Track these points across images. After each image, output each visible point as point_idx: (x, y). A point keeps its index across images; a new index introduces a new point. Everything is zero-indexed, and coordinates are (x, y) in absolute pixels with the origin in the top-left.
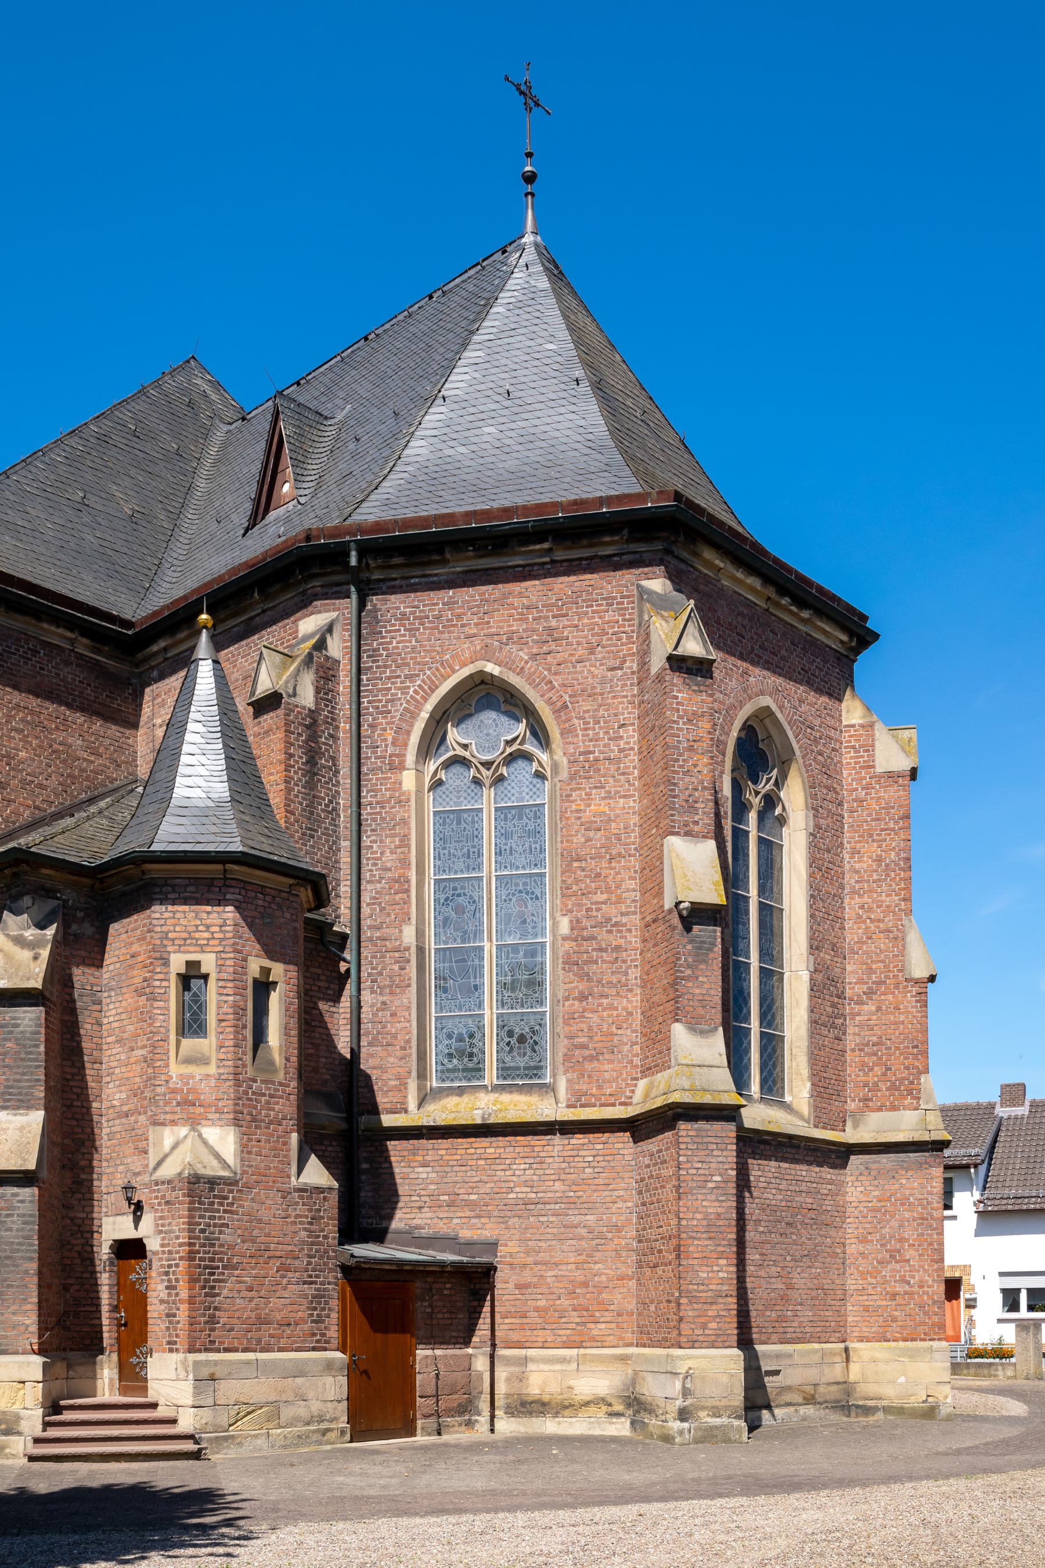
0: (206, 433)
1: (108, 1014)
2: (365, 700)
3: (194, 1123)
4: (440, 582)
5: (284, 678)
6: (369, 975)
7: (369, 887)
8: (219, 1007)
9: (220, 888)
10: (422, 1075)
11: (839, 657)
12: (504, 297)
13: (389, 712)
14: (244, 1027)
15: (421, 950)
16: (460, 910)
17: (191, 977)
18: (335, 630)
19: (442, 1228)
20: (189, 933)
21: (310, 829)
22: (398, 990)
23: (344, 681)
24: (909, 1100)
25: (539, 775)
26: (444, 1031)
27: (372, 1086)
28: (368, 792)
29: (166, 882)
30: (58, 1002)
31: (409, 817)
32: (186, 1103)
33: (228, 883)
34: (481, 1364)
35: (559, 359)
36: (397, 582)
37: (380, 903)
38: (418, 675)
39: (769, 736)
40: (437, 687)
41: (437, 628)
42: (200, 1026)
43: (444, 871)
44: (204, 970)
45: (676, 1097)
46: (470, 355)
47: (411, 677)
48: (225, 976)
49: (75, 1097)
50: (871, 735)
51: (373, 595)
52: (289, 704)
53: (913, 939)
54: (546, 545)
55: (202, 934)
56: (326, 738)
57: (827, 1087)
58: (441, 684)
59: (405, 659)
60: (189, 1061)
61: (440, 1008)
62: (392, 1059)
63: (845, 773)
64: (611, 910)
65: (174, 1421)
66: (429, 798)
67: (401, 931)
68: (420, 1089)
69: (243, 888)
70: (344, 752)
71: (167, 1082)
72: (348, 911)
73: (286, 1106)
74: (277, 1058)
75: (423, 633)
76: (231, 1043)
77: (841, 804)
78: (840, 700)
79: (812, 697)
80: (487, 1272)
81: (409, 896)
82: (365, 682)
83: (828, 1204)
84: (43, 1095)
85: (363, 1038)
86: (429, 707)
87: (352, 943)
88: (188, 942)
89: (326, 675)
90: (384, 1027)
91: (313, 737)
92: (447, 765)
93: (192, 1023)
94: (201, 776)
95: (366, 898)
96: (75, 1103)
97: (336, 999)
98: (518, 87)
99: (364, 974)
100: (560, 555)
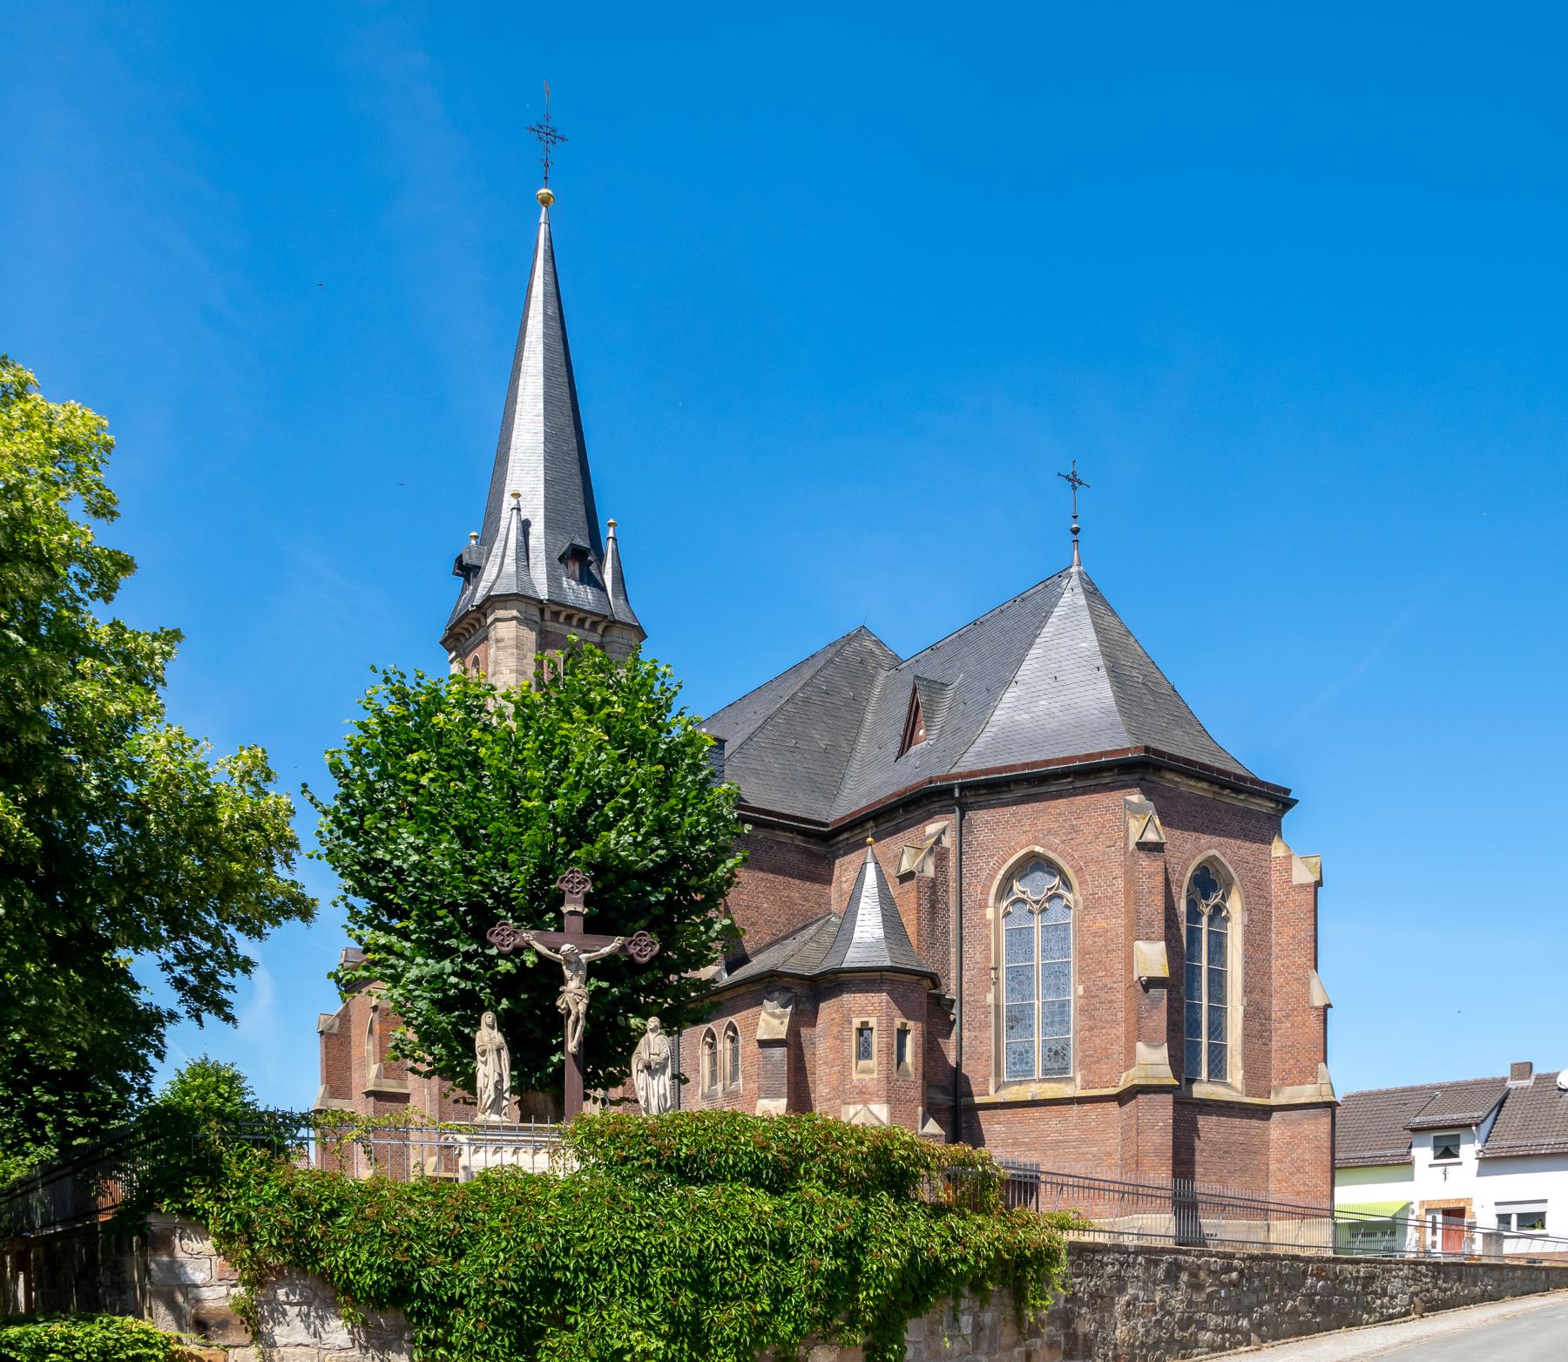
0: (872, 679)
3: (865, 1103)
10: (998, 1074)
11: (1269, 817)
12: (1058, 611)
15: (997, 1007)
16: (1021, 983)
17: (864, 1029)
25: (1067, 907)
29: (850, 982)
30: (794, 1045)
45: (1136, 1082)
46: (1034, 652)
47: (991, 856)
50: (1292, 857)
53: (1314, 983)
55: (871, 1009)
57: (1256, 1073)
60: (862, 1072)
64: (1108, 981)
66: (1003, 922)
70: (953, 899)
73: (916, 1093)
78: (1270, 843)
79: (1248, 844)
83: (1256, 1141)
86: (1002, 872)
87: (957, 1004)
92: (1013, 903)
94: (868, 926)
95: (965, 979)
97: (948, 1036)
100: (1078, 784)
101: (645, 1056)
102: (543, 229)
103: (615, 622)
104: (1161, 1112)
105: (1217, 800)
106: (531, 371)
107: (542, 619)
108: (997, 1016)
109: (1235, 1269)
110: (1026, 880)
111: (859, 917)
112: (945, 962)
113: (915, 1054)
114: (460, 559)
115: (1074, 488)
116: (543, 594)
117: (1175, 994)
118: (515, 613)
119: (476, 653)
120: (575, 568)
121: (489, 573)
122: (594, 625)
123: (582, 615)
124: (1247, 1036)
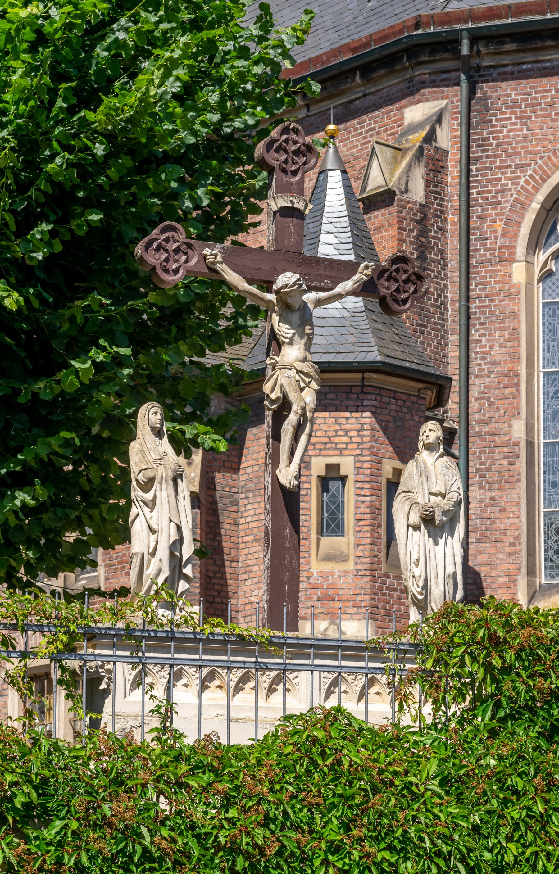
1: (245, 514)
2: (474, 191)
4: (553, 68)
5: (397, 174)
6: (478, 470)
7: (478, 381)
8: (357, 507)
9: (358, 394)
10: (531, 572)
13: (499, 203)
14: (379, 525)
15: (530, 444)
18: (444, 120)
20: (329, 438)
21: (421, 325)
22: (507, 486)
23: (452, 172)
26: (554, 526)
27: (481, 583)
28: (477, 285)
31: (519, 310)
32: (326, 598)
33: (366, 389)
36: (509, 69)
37: (489, 398)
38: (529, 165)
40: (549, 177)
41: (549, 115)
42: (338, 526)
43: (554, 363)
44: (343, 472)
47: (522, 167)
48: (361, 477)
49: (216, 593)
51: (482, 82)
52: (401, 201)
56: (435, 232)
58: (553, 173)
59: (516, 148)
60: (328, 558)
61: (549, 503)
62: (501, 556)
67: (510, 426)
68: (530, 585)
69: (379, 394)
70: (453, 245)
71: (308, 578)
72: (455, 406)
75: (535, 122)
76: (368, 541)
81: (518, 391)
82: (474, 172)
84: (198, 591)
85: (471, 534)
86: (540, 197)
88: (328, 446)
89: (436, 169)
90: (493, 523)
91: (424, 232)
95: (474, 392)
96: (216, 600)
101: (421, 498)
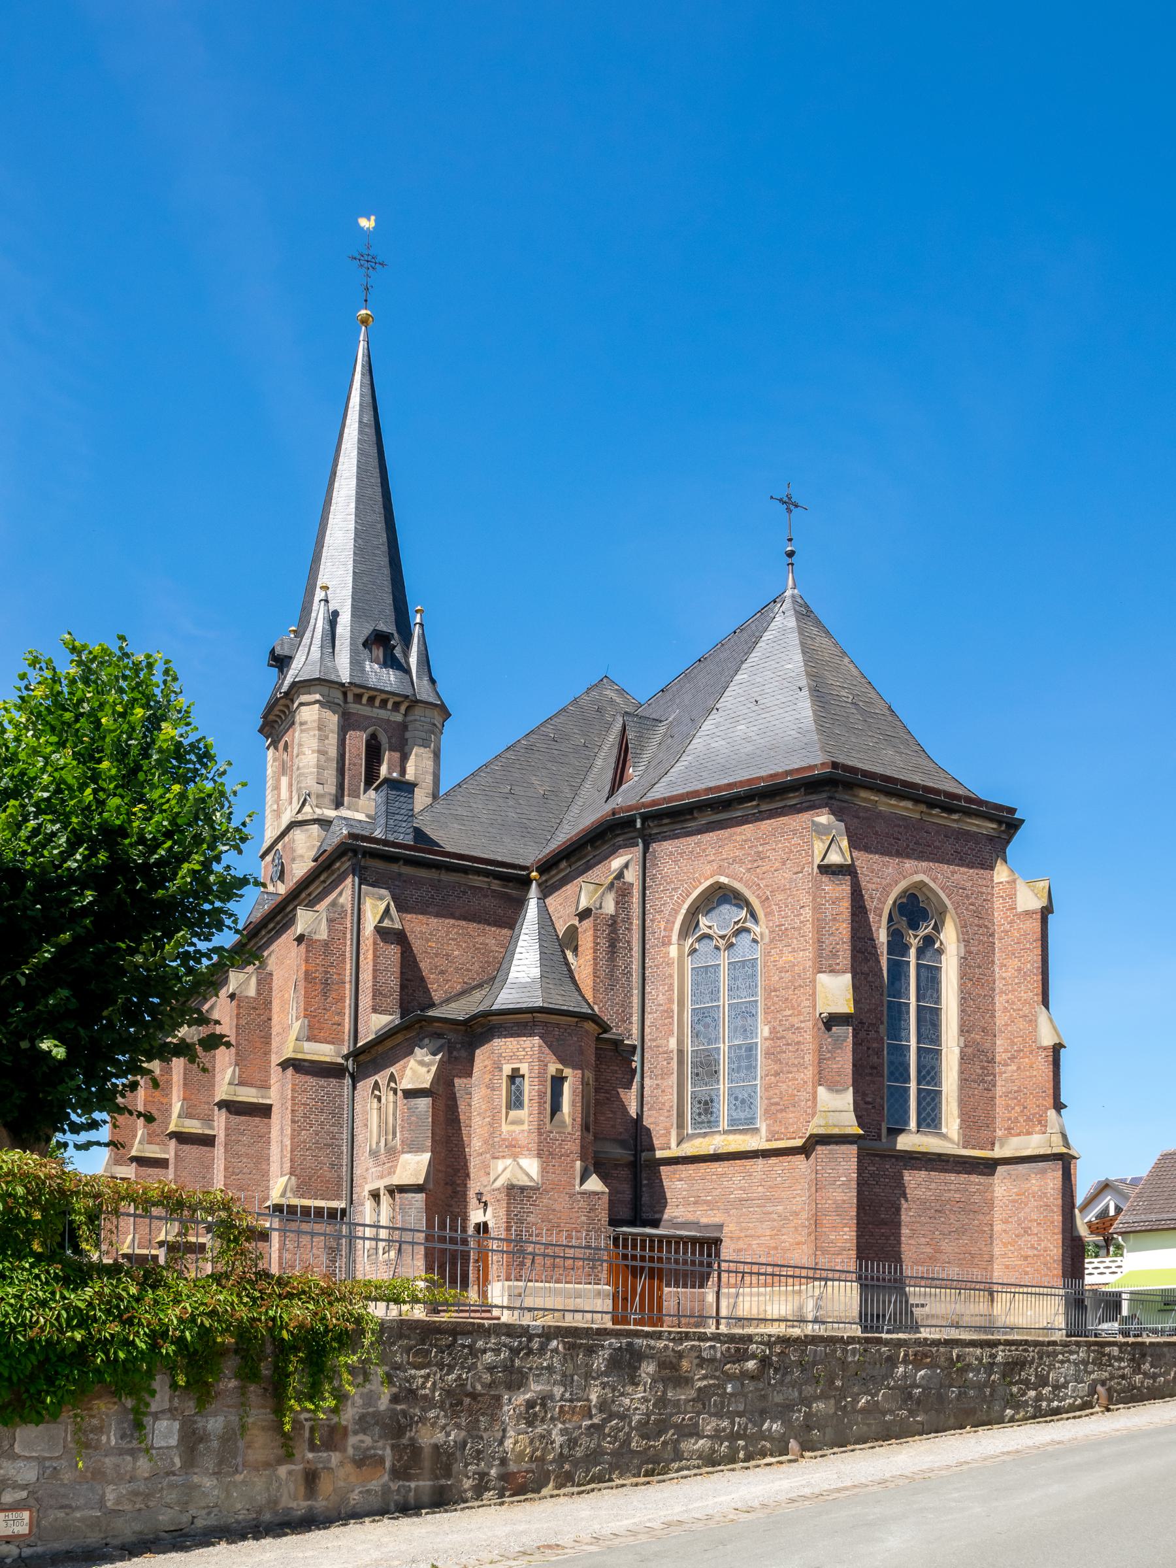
3: (515, 1157)
10: (681, 1126)
12: (767, 636)
15: (681, 1052)
16: (706, 1026)
19: (691, 1217)
24: (1038, 1128)
25: (754, 941)
34: (711, 1298)
35: (793, 674)
39: (928, 898)
47: (675, 889)
54: (754, 803)
55: (520, 1054)
57: (977, 1120)
60: (513, 1123)
61: (694, 1085)
63: (996, 914)
65: (499, 1319)
73: (573, 1146)
74: (567, 1119)
77: (992, 935)
78: (992, 868)
79: (963, 869)
80: (717, 1242)
83: (976, 1198)
86: (686, 906)
87: (638, 1051)
92: (699, 939)
93: (515, 1102)
95: (647, 1023)
97: (628, 1086)
98: (781, 500)
99: (646, 1068)
100: (764, 807)
102: (362, 346)
103: (418, 701)
104: (846, 1161)
105: (912, 820)
106: (346, 474)
107: (346, 701)
108: (681, 1062)
109: (754, 1356)
110: (714, 914)
111: (517, 956)
112: (626, 1005)
113: (573, 1104)
114: (273, 651)
115: (789, 511)
116: (345, 678)
117: (862, 1034)
118: (318, 697)
119: (286, 738)
120: (379, 653)
121: (296, 664)
122: (397, 705)
123: (384, 696)
124: (965, 1080)
